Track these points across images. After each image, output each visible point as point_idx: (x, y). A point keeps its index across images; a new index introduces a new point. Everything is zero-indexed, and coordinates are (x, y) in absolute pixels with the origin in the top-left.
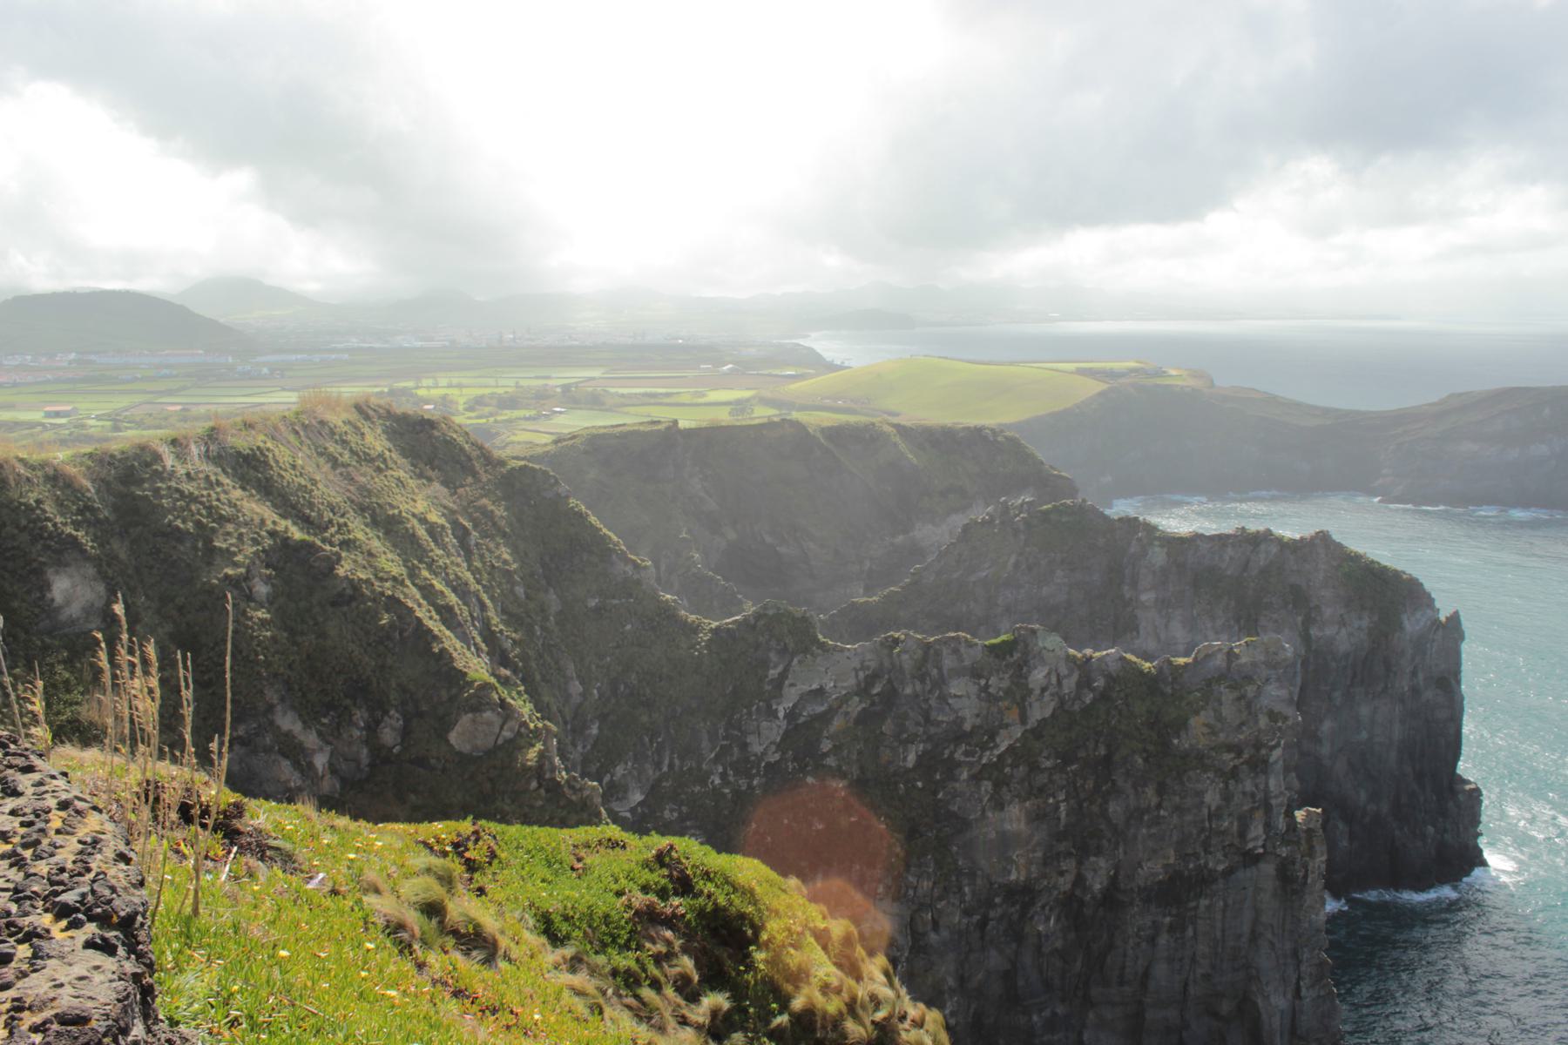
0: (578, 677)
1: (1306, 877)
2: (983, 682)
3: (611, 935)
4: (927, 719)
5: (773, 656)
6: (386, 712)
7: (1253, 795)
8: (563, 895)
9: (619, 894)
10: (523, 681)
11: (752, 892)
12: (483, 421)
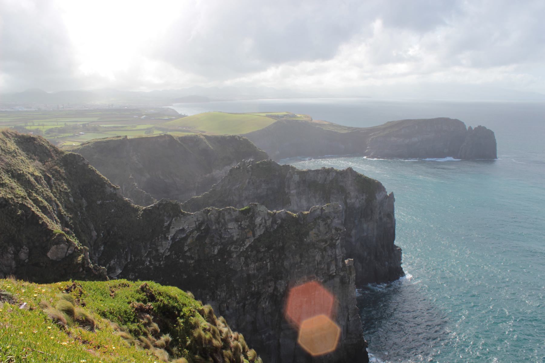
0: (95, 229)
1: (349, 282)
2: (239, 223)
3: (128, 318)
4: (221, 237)
5: (166, 218)
6: (22, 247)
7: (331, 256)
8: (108, 305)
9: (129, 303)
10: (75, 232)
11: (176, 298)
12: (53, 138)
